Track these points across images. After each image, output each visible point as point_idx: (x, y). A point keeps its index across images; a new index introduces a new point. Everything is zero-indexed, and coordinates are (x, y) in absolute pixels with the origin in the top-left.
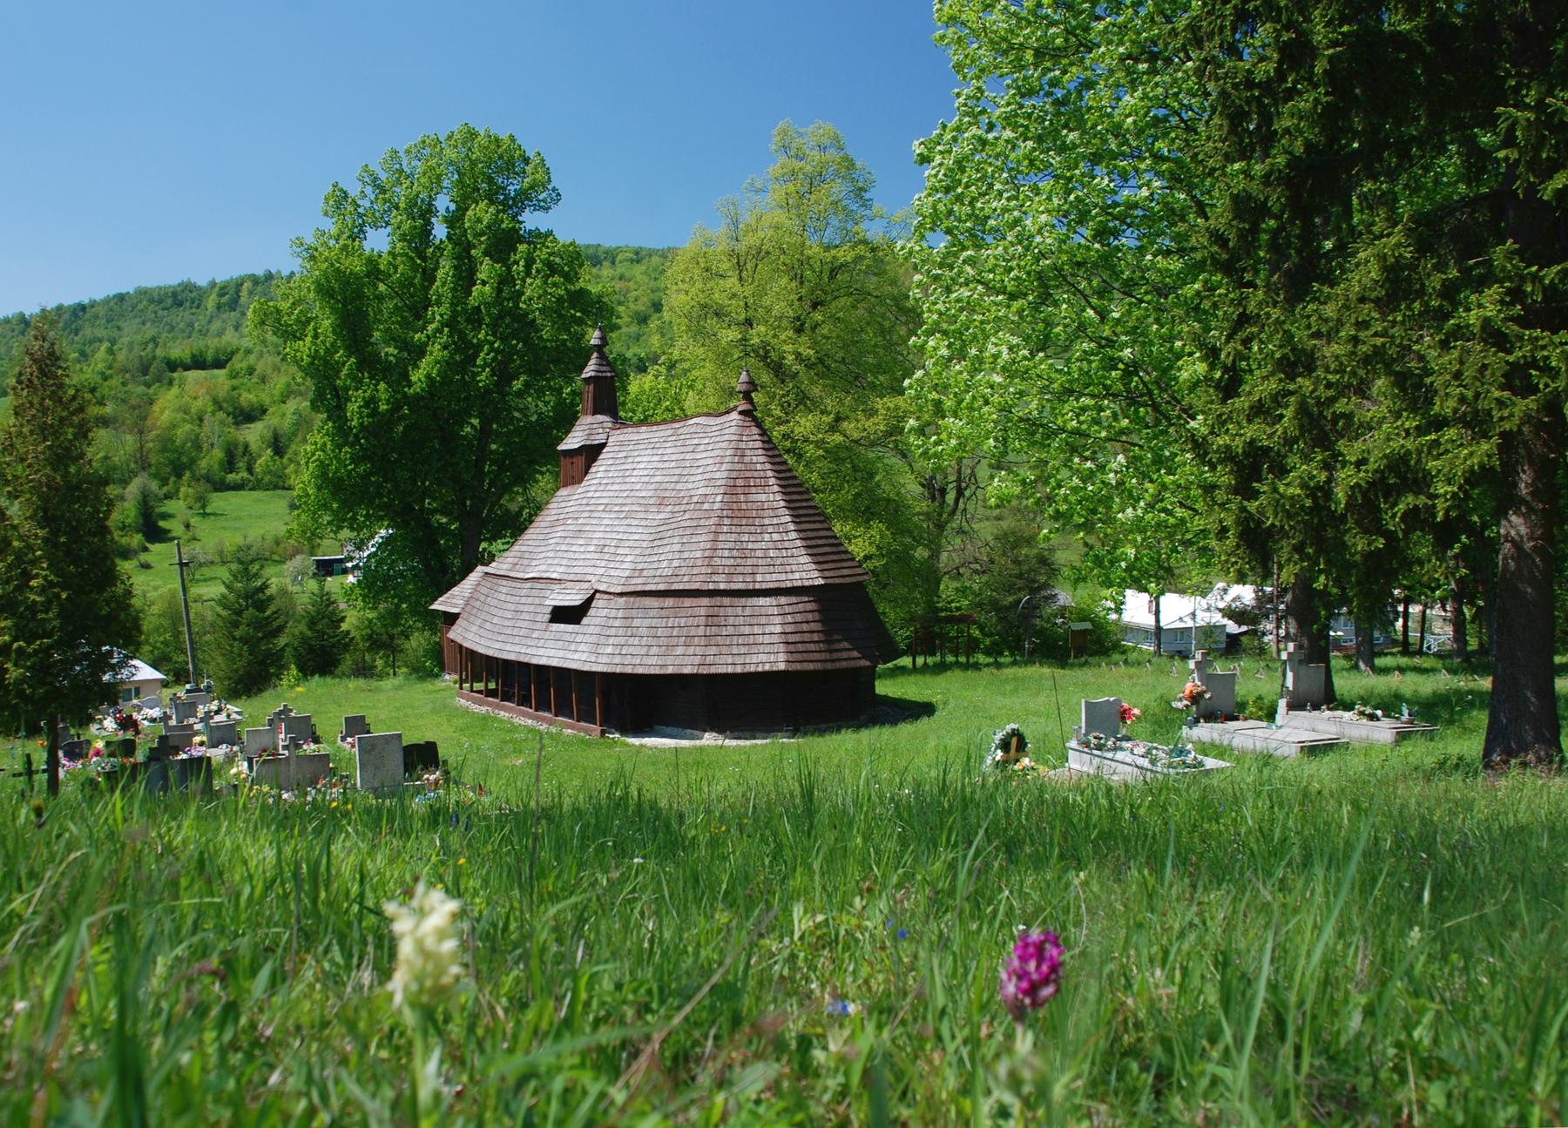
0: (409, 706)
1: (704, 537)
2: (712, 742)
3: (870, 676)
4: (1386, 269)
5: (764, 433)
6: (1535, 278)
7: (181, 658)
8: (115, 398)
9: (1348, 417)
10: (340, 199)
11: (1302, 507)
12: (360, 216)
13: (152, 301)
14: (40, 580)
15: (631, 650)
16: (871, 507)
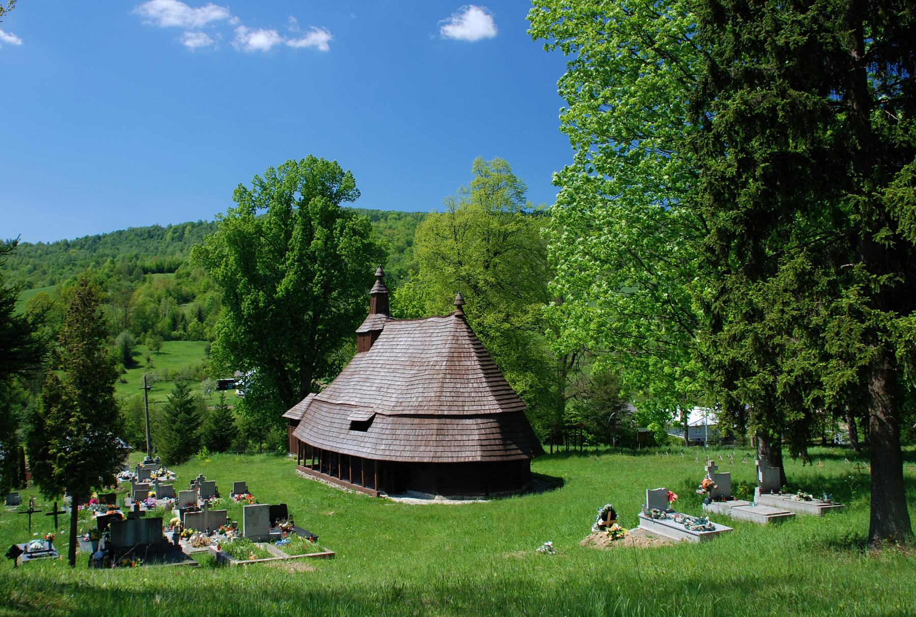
0: (272, 477)
1: (436, 385)
2: (439, 502)
3: (527, 464)
4: (796, 275)
5: (469, 328)
6: (875, 281)
7: (141, 435)
8: (113, 288)
9: (782, 346)
10: (242, 193)
11: (760, 395)
12: (253, 201)
13: (136, 235)
14: (75, 419)
15: (395, 447)
16: (526, 364)
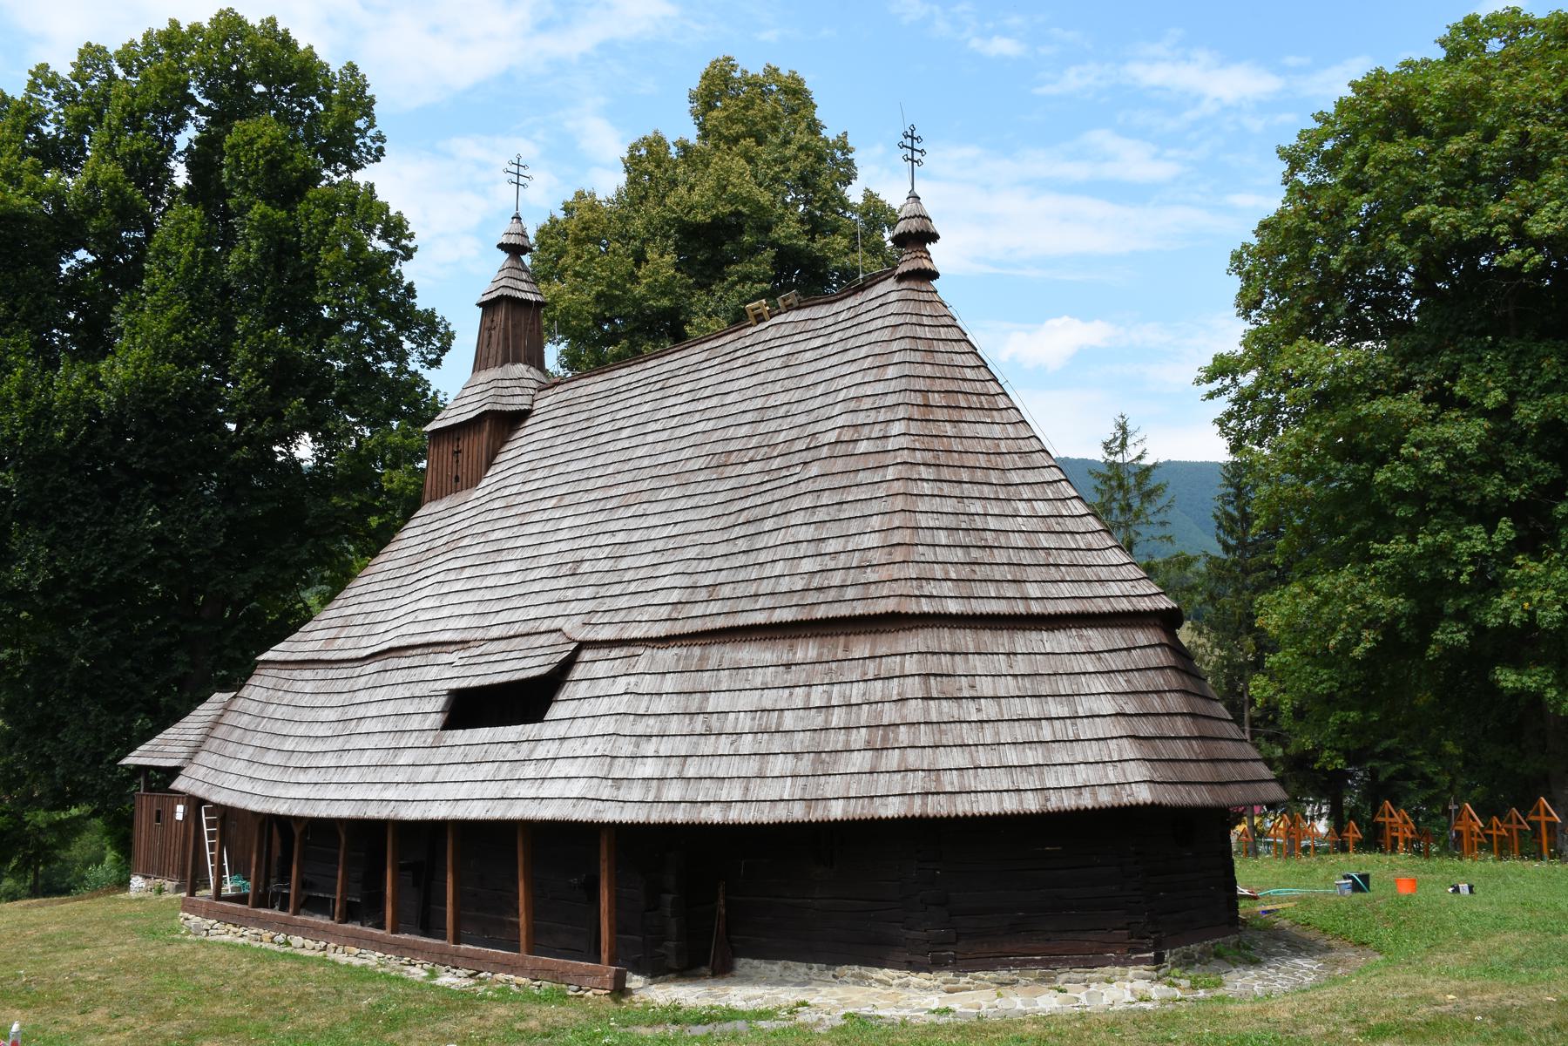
10: (31, 72)
